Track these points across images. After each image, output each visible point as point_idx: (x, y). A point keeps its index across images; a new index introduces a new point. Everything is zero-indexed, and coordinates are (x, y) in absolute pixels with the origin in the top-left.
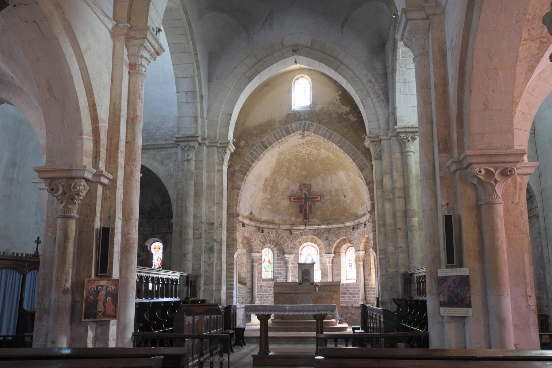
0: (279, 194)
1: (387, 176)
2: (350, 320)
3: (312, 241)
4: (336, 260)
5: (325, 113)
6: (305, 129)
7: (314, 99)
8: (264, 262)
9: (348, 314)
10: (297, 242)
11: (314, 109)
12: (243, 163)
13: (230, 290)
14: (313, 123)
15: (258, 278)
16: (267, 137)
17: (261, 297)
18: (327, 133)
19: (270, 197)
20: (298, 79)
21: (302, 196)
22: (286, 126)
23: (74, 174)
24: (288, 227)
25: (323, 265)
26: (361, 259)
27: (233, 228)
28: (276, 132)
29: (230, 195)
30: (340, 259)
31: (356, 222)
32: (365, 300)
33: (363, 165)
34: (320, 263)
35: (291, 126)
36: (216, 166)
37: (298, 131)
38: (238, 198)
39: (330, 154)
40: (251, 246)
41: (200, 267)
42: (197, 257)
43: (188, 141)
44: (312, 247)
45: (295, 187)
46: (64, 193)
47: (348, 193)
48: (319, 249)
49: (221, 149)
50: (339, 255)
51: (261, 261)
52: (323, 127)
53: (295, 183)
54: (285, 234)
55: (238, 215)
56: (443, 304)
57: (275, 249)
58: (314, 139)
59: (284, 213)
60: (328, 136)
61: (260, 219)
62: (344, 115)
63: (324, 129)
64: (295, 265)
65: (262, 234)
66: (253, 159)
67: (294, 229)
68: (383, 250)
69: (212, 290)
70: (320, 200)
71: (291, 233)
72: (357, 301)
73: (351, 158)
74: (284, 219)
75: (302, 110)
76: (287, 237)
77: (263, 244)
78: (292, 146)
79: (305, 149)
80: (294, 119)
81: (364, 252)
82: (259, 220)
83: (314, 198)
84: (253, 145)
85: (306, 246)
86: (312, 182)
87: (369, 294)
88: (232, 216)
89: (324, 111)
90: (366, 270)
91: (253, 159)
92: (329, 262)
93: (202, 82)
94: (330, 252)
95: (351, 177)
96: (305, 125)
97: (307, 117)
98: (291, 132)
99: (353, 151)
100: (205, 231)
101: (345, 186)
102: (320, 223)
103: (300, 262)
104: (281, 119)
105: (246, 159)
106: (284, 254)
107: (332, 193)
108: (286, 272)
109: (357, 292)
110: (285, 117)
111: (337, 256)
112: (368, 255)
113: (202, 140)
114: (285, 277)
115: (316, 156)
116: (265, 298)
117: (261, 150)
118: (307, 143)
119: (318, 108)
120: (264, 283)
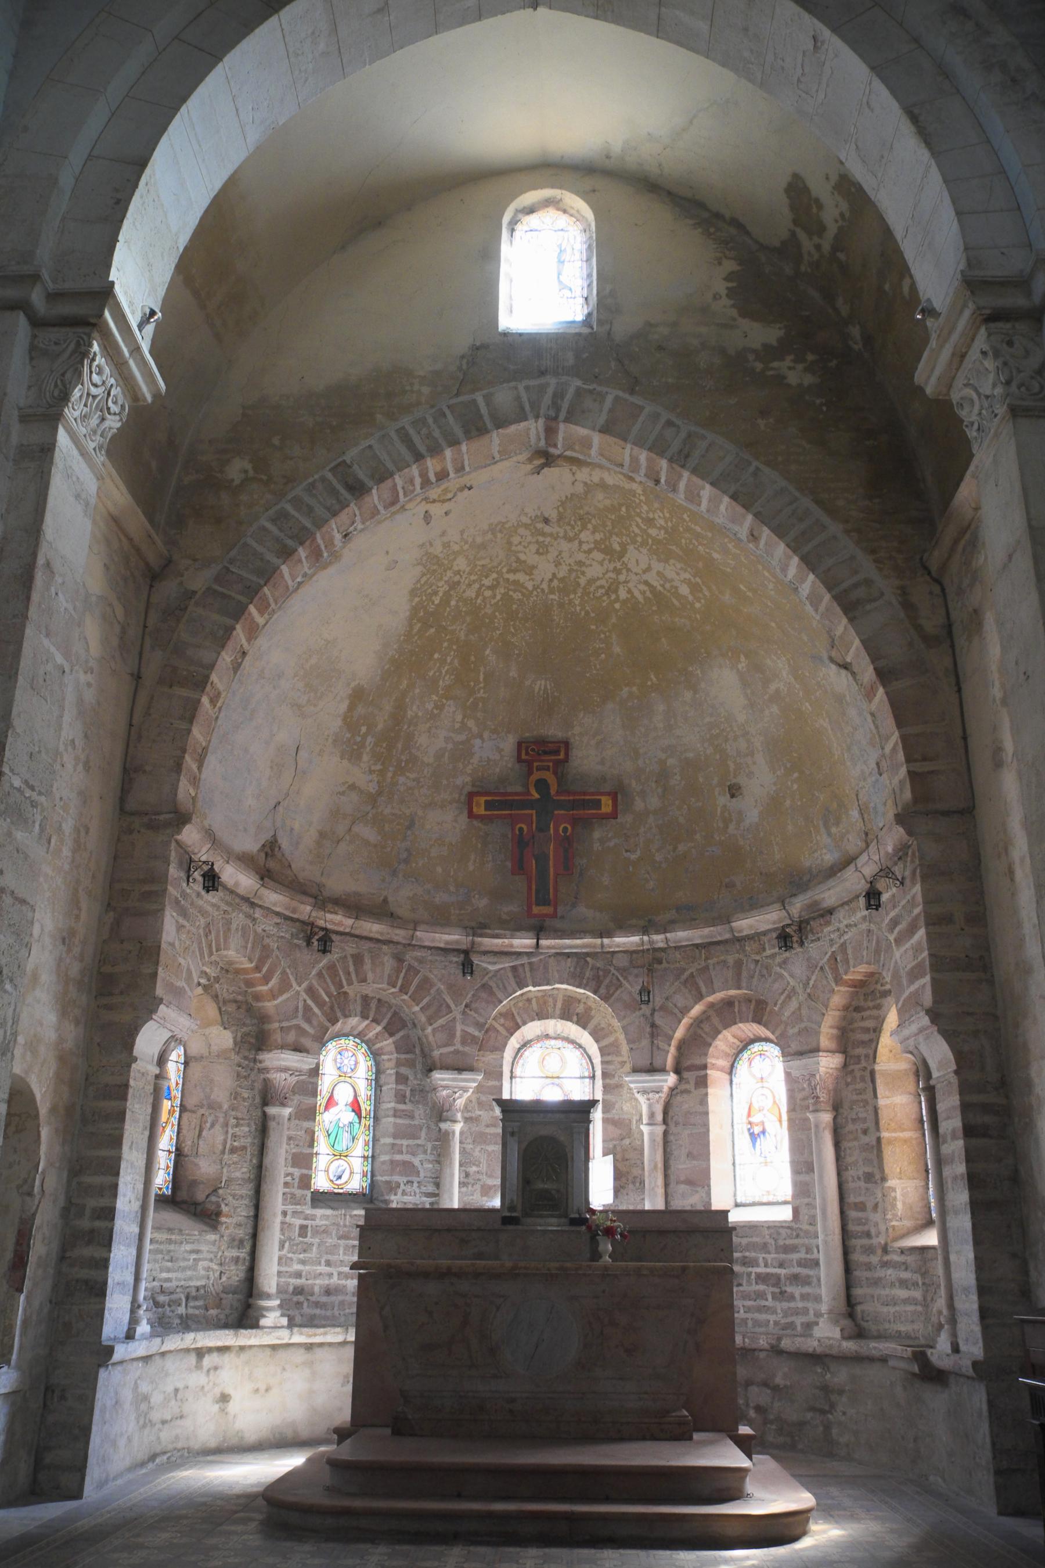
2: (766, 1421)
3: (566, 1015)
4: (686, 1106)
6: (558, 410)
7: (608, 288)
8: (327, 1108)
9: (754, 1390)
11: (607, 327)
13: (89, 1242)
14: (599, 388)
15: (286, 1184)
16: (364, 444)
19: (373, 788)
21: (528, 793)
24: (457, 937)
26: (823, 1096)
27: (147, 888)
28: (414, 423)
30: (704, 1101)
33: (856, 586)
35: (488, 398)
37: (525, 419)
38: (189, 731)
44: (566, 1044)
47: (750, 775)
48: (601, 1049)
50: (702, 1082)
51: (308, 1101)
52: (649, 409)
55: (182, 819)
57: (387, 1044)
58: (603, 485)
59: (439, 870)
61: (320, 886)
62: (751, 357)
63: (656, 416)
65: (325, 960)
66: (290, 542)
67: (485, 953)
71: (467, 967)
72: (799, 1321)
73: (795, 551)
74: (437, 900)
76: (450, 987)
77: (324, 1014)
78: (492, 530)
79: (551, 556)
83: (584, 804)
86: (577, 730)
87: (876, 1282)
88: (146, 819)
90: (854, 1156)
91: (290, 542)
92: (652, 1115)
94: (657, 1063)
95: (773, 687)
96: (558, 396)
98: (489, 424)
101: (735, 739)
103: (506, 1096)
108: (439, 1162)
109: (797, 1270)
110: (463, 357)
111: (691, 1086)
112: (858, 1074)
114: (431, 1188)
115: (601, 591)
118: (561, 518)
119: (624, 326)
120: (319, 1212)
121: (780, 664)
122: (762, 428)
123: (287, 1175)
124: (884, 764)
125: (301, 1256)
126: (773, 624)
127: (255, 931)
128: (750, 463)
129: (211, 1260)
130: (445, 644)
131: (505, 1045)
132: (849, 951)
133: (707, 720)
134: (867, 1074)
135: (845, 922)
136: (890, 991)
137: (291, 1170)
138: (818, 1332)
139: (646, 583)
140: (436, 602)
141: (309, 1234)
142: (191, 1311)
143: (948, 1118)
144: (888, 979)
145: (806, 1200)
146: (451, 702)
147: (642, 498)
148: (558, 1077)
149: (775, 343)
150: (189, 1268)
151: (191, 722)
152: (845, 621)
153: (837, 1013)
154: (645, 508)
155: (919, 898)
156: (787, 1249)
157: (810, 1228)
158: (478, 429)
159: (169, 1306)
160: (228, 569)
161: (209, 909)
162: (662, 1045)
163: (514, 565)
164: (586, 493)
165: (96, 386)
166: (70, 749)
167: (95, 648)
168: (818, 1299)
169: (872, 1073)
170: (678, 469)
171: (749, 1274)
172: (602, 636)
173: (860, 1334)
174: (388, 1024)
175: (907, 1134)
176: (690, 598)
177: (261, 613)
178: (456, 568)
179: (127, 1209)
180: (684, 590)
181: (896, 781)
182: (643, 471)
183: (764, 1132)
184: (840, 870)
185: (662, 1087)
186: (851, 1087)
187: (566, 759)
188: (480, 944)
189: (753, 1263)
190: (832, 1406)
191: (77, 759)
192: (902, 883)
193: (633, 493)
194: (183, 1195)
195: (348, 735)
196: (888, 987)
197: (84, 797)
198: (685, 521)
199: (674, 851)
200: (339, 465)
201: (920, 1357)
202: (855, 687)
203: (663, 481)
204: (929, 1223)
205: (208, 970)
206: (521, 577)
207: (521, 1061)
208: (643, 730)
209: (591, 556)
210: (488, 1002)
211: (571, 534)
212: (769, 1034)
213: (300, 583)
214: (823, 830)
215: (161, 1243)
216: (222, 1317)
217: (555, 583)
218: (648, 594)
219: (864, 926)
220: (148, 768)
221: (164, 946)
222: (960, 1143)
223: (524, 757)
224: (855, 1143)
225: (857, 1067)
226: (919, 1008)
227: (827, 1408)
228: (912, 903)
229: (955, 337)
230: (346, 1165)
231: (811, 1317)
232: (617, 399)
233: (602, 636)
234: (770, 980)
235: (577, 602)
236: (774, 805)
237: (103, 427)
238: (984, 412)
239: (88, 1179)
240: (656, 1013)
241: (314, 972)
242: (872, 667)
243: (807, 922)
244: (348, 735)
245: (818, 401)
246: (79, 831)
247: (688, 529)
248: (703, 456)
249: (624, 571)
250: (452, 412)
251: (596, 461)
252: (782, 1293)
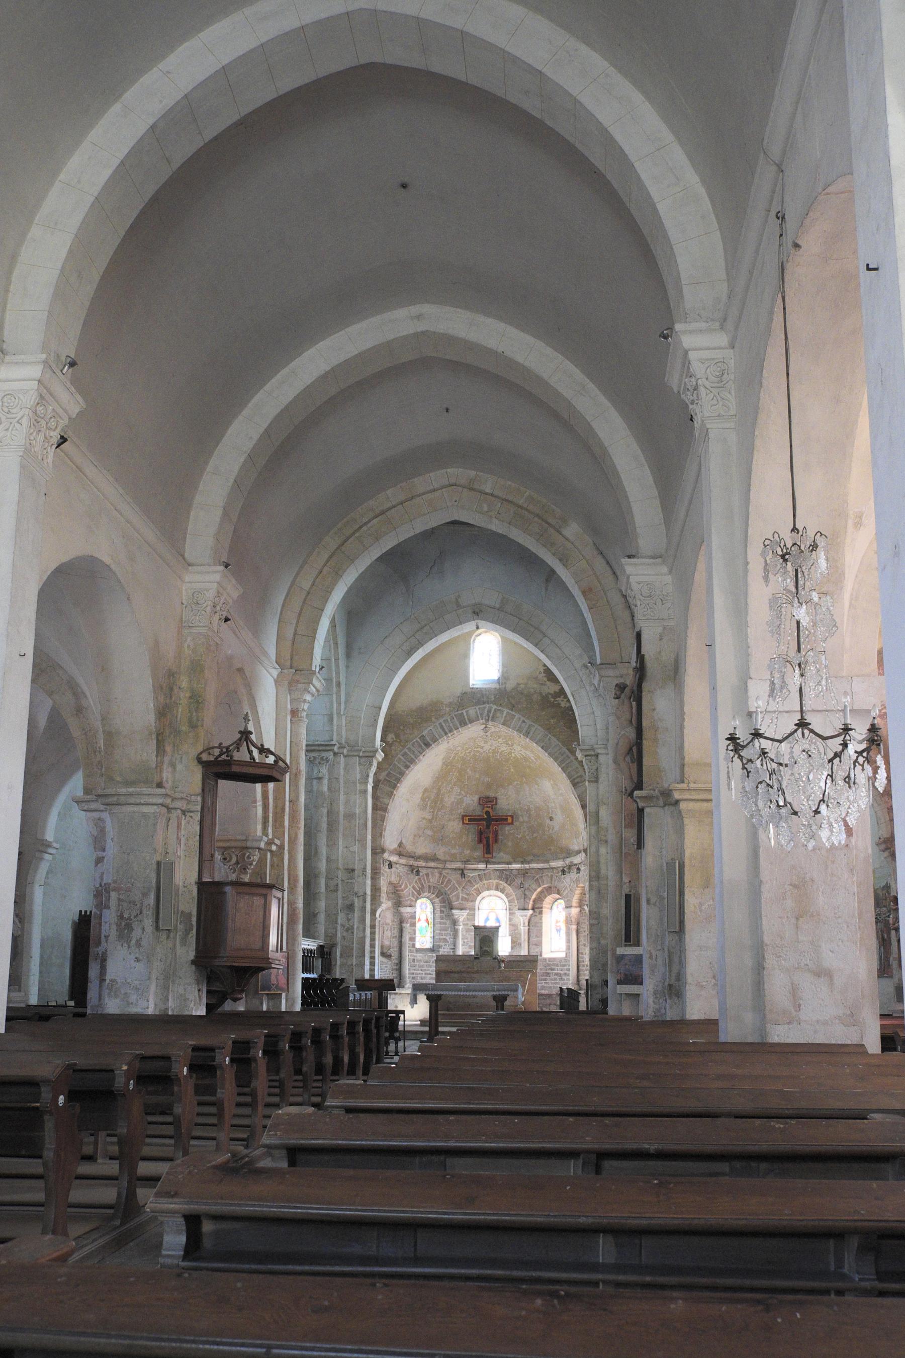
1: (604, 807)
3: (497, 889)
5: (522, 693)
6: (489, 717)
10: (472, 890)
18: (523, 725)
20: (480, 635)
22: (460, 712)
23: (249, 844)
25: (513, 927)
26: (574, 920)
30: (541, 919)
31: (568, 861)
32: (578, 984)
33: (578, 777)
34: (510, 925)
35: (467, 712)
36: (358, 785)
39: (528, 753)
40: (399, 897)
41: (336, 931)
42: (332, 919)
43: (320, 751)
45: (471, 802)
46: (237, 863)
47: (556, 815)
49: (363, 760)
50: (541, 913)
52: (517, 716)
54: (455, 877)
56: (620, 982)
57: (437, 900)
60: (525, 729)
61: (415, 853)
62: (550, 696)
64: (469, 927)
65: (417, 877)
66: (408, 763)
68: (595, 913)
69: (352, 965)
70: (512, 823)
71: (463, 875)
75: (485, 686)
81: (578, 910)
85: (488, 896)
91: (408, 763)
92: (524, 924)
94: (526, 907)
96: (489, 711)
100: (342, 880)
102: (512, 860)
106: (451, 909)
111: (537, 914)
113: (339, 748)
119: (510, 685)
120: (418, 955)
187: (496, 804)
189: (553, 969)
206: (479, 749)
232: (508, 712)
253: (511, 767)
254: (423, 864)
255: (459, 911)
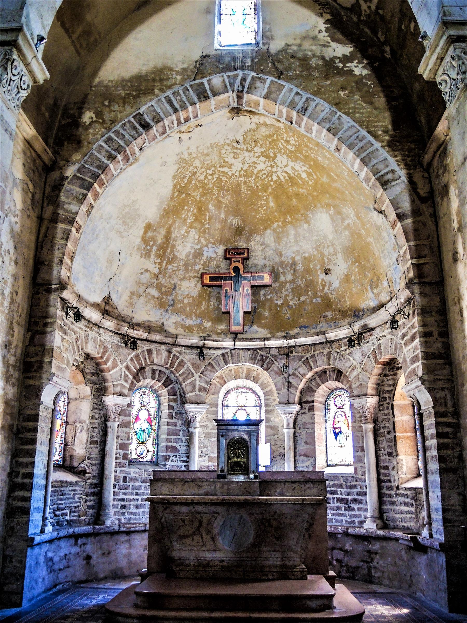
0: (177, 267)
3: (248, 377)
6: (243, 87)
9: (336, 551)
10: (215, 377)
12: (85, 162)
13: (21, 490)
14: (263, 76)
15: (116, 458)
16: (149, 104)
17: (123, 507)
18: (297, 98)
19: (156, 271)
21: (229, 273)
22: (198, 81)
26: (369, 416)
29: (46, 236)
33: (387, 173)
35: (209, 81)
38: (66, 245)
47: (335, 264)
48: (264, 393)
50: (312, 409)
52: (288, 86)
53: (214, 244)
55: (63, 286)
58: (265, 125)
59: (188, 309)
61: (132, 318)
62: (337, 61)
63: (291, 90)
65: (134, 353)
66: (113, 153)
67: (210, 348)
71: (201, 355)
72: (357, 520)
76: (194, 364)
78: (212, 146)
79: (240, 159)
80: (218, 67)
82: (128, 320)
84: (113, 122)
87: (393, 503)
89: (291, 51)
90: (384, 444)
91: (113, 153)
92: (288, 424)
93: (242, 593)
94: (291, 401)
95: (346, 222)
96: (244, 80)
97: (249, 62)
98: (210, 94)
99: (361, 141)
101: (328, 247)
103: (220, 418)
104: (185, 66)
105: (94, 152)
107: (298, 268)
108: (189, 446)
109: (356, 497)
110: (197, 61)
111: (306, 411)
112: (385, 406)
114: (185, 459)
115: (264, 176)
116: (132, 509)
117: (134, 132)
118: (245, 140)
121: (349, 211)
122: (342, 96)
123: (117, 454)
124: (400, 260)
125: (124, 491)
126: (347, 192)
127: (101, 340)
128: (336, 113)
129: (81, 494)
130: (190, 202)
131: (219, 391)
132: (382, 348)
133: (315, 238)
134: (390, 406)
135: (380, 335)
136: (401, 367)
137: (119, 451)
138: (366, 526)
139: (286, 172)
140: (186, 182)
141: (128, 481)
142: (72, 518)
143: (429, 429)
144: (401, 362)
145: (361, 464)
146: (193, 230)
147: (284, 130)
148: (244, 406)
149: (348, 54)
150: (71, 498)
151: (67, 240)
152: (382, 190)
153: (376, 377)
154: (285, 135)
155: (416, 324)
156: (352, 487)
157: (363, 477)
158: (204, 97)
159: (62, 516)
160: (84, 166)
161: (77, 329)
162: (293, 391)
163: (223, 164)
164: (257, 128)
165: (14, 75)
166: (7, 254)
167: (19, 205)
168: (366, 510)
169: (392, 405)
170: (302, 116)
171: (333, 498)
172: (265, 198)
173: (385, 526)
174: (164, 382)
175: (409, 434)
176: (307, 179)
177: (101, 187)
178: (194, 165)
179: (39, 473)
180: (304, 175)
181: (405, 268)
182: (284, 117)
183: (340, 432)
184: (378, 310)
185: (293, 411)
186: (382, 412)
188: (208, 344)
190: (372, 560)
191: (11, 259)
192: (408, 317)
193: (279, 128)
194: (68, 463)
195: (144, 246)
196: (400, 365)
197: (15, 278)
198: (304, 141)
199: (299, 300)
200: (137, 114)
201: (414, 540)
202: (386, 222)
203: (294, 122)
204: (419, 475)
205: (78, 359)
206: (226, 169)
207: (227, 399)
208: (284, 243)
209: (260, 159)
210: (211, 371)
211: (250, 149)
212: (343, 387)
213: (119, 173)
214: (370, 290)
215: (57, 487)
216: (87, 520)
217: (242, 172)
218: (287, 178)
219: (389, 337)
220: (46, 263)
221: (55, 348)
222: (435, 441)
223: (228, 256)
224: (384, 438)
225: (385, 402)
226: (416, 377)
227: (370, 560)
228: (413, 326)
229: (438, 50)
230: (145, 448)
231: (362, 519)
233: (265, 198)
234: (344, 361)
235: (253, 182)
236: (347, 279)
237: (18, 96)
238: (452, 87)
239: (21, 460)
240: (290, 377)
241: (129, 358)
242: (395, 213)
243: (362, 334)
244: (144, 246)
245: (369, 83)
246: (13, 294)
247: (307, 146)
248: (313, 110)
249: (275, 167)
250: (192, 88)
251: (262, 112)
252: (349, 507)
253: (271, 199)
254: (145, 335)
255: (196, 405)
